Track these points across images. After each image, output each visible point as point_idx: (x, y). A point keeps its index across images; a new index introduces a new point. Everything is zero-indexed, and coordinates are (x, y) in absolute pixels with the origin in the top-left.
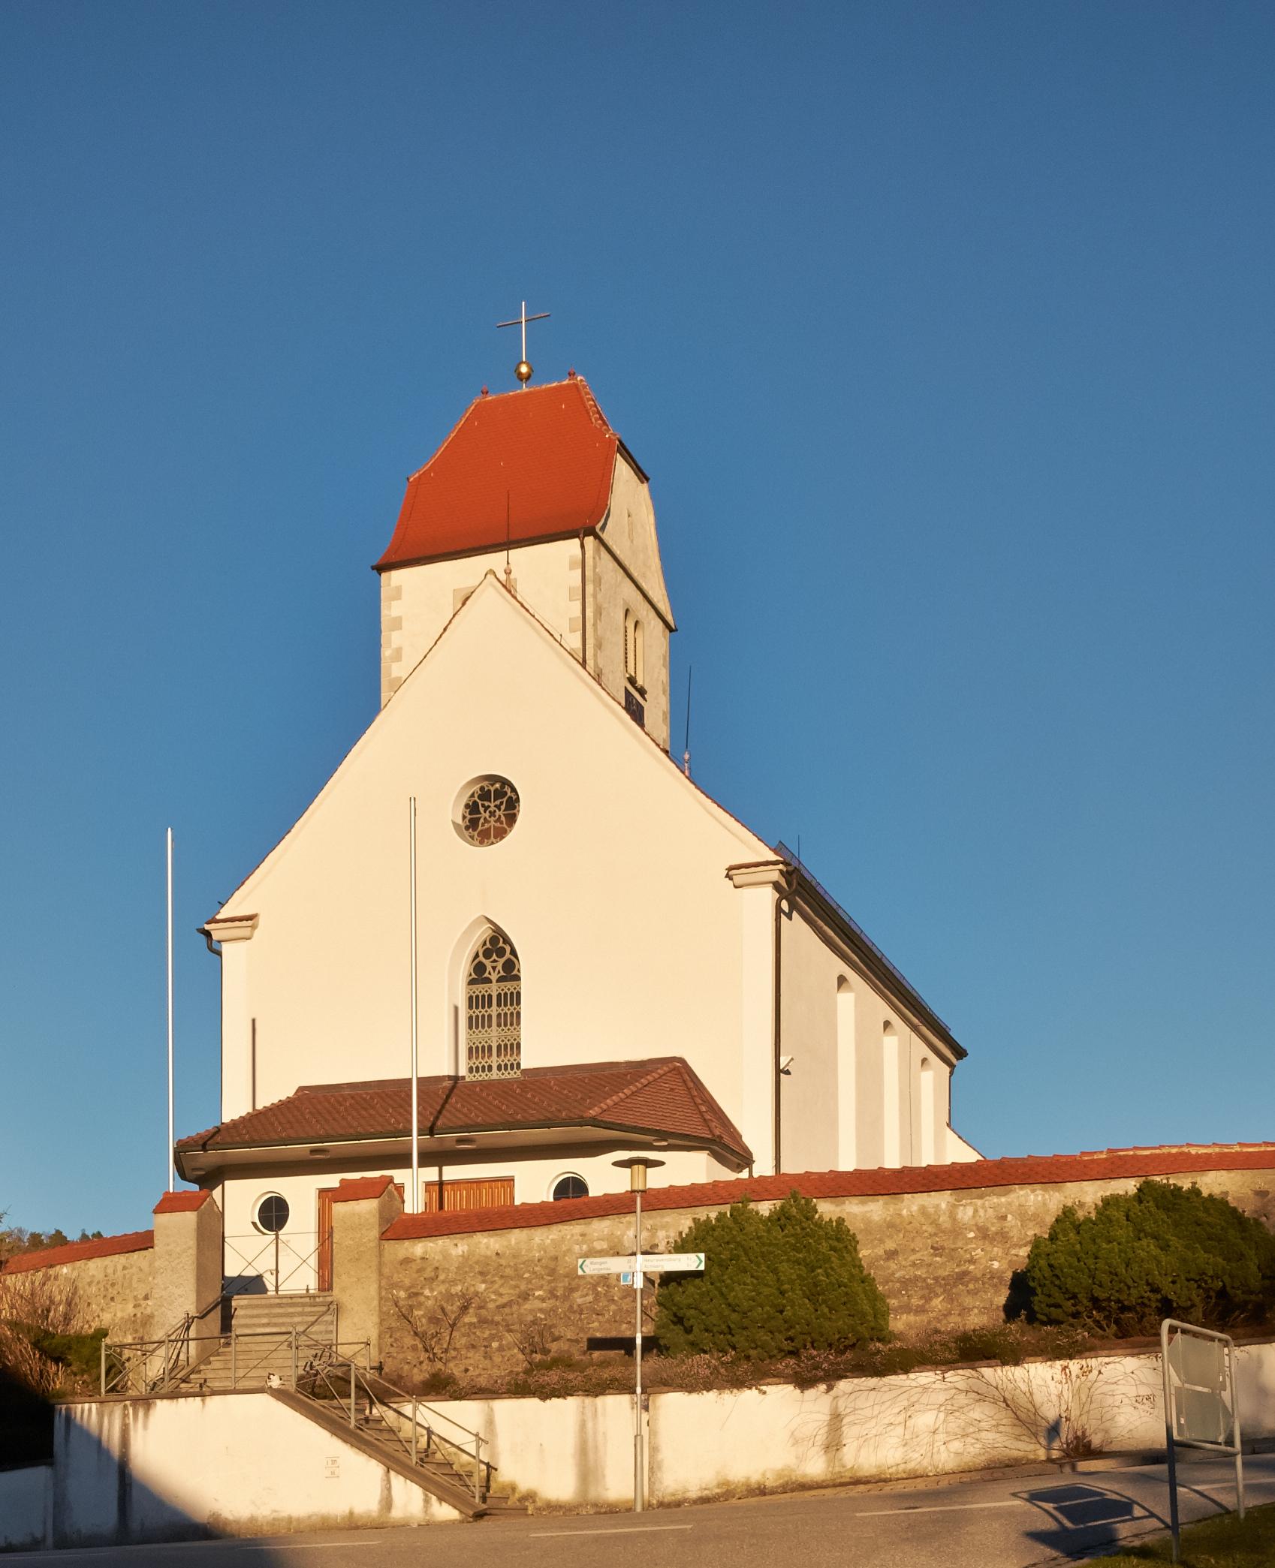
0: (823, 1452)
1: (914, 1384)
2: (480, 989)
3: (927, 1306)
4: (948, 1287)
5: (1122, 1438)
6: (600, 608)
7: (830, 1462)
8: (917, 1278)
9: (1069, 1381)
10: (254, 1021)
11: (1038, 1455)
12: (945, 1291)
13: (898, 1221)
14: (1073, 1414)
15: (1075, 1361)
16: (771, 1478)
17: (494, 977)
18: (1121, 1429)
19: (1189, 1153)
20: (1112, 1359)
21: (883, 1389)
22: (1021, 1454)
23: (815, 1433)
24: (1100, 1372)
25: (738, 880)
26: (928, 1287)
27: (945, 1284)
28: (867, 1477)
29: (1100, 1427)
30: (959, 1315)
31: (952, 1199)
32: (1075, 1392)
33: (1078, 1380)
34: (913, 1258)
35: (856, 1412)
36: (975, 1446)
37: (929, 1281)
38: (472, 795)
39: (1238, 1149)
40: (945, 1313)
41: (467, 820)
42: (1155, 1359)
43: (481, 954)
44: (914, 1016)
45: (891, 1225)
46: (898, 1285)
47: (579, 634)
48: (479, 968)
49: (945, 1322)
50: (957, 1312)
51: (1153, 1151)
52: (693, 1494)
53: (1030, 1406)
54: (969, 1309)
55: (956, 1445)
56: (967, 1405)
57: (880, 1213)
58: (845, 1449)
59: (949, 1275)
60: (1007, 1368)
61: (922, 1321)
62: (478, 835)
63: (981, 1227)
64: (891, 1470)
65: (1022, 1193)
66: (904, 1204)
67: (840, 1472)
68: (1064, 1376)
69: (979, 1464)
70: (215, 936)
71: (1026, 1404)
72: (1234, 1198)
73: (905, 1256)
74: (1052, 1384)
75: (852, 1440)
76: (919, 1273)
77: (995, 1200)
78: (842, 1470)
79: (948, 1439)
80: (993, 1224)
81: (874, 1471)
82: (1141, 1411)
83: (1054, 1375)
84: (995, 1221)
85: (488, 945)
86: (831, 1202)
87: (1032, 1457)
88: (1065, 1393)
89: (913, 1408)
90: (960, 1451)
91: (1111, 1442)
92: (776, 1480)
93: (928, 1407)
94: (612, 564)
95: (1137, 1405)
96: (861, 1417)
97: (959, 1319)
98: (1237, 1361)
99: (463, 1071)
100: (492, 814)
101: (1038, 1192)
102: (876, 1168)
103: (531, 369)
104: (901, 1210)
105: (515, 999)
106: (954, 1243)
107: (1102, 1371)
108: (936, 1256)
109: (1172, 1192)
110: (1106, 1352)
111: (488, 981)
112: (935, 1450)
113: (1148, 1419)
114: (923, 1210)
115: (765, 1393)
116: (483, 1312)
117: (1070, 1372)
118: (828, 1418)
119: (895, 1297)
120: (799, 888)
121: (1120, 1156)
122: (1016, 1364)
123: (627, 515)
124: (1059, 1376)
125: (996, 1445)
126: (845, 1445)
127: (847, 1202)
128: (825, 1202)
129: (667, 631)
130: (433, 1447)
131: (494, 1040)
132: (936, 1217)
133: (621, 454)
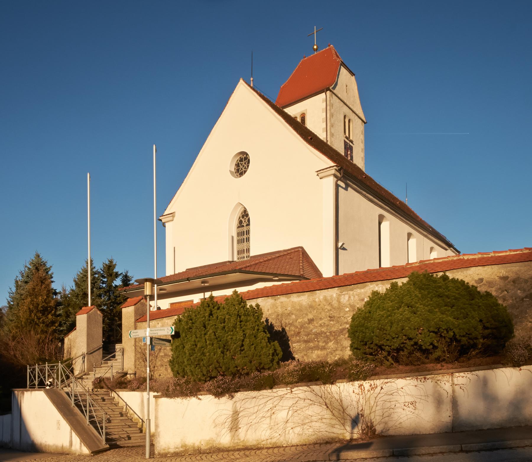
0: (229, 431)
1: (275, 395)
2: (241, 229)
3: (326, 346)
4: (336, 337)
5: (395, 427)
6: (333, 114)
7: (233, 436)
8: (322, 332)
9: (363, 393)
10: (174, 248)
11: (345, 437)
12: (334, 338)
13: (314, 304)
14: (365, 413)
15: (367, 381)
16: (203, 445)
17: (245, 225)
18: (394, 422)
19: (464, 259)
20: (389, 380)
21: (259, 398)
22: (335, 435)
23: (225, 421)
24: (382, 388)
25: (321, 175)
26: (327, 337)
27: (335, 335)
28: (251, 446)
29: (382, 421)
30: (341, 350)
31: (338, 292)
32: (367, 400)
33: (369, 392)
34: (320, 322)
35: (246, 410)
36: (309, 430)
37: (328, 334)
38: (237, 161)
39: (493, 255)
40: (335, 349)
41: (236, 170)
42: (416, 380)
43: (241, 217)
44: (424, 231)
45: (311, 307)
46: (313, 336)
47: (325, 123)
48: (241, 222)
49: (334, 354)
50: (340, 349)
51: (444, 260)
52: (172, 450)
53: (340, 408)
54: (345, 347)
55: (298, 430)
56: (305, 407)
57: (306, 301)
58: (240, 430)
59: (337, 330)
60: (327, 385)
61: (324, 354)
62: (239, 174)
63: (352, 305)
64: (263, 443)
65: (371, 286)
66: (317, 296)
67: (237, 443)
68: (360, 391)
69: (311, 441)
70: (163, 221)
71: (338, 406)
72: (486, 282)
73: (317, 322)
74: (353, 395)
75: (244, 425)
76: (323, 330)
77: (359, 291)
78: (239, 442)
79: (294, 426)
80: (358, 303)
81: (254, 443)
82: (407, 411)
83: (354, 390)
84: (359, 302)
85: (243, 214)
86: (285, 297)
87: (341, 437)
88: (361, 400)
89: (275, 408)
90: (300, 433)
91: (389, 430)
92: (206, 446)
93: (284, 408)
94: (338, 100)
95: (405, 407)
96: (248, 413)
97: (341, 353)
98: (470, 381)
99: (236, 259)
100: (243, 166)
101: (380, 285)
102: (184, 270)
103: (318, 47)
104: (315, 299)
105: (248, 232)
106: (339, 314)
107: (383, 388)
108: (331, 321)
109: (460, 282)
110: (385, 376)
111: (243, 226)
112: (287, 432)
113: (412, 416)
114: (325, 299)
115: (201, 399)
116: (165, 351)
117: (364, 388)
118: (231, 413)
119: (312, 342)
120: (345, 175)
121: (426, 264)
122: (332, 383)
123: (345, 86)
124: (357, 390)
125: (321, 430)
126: (240, 428)
127: (292, 296)
128: (283, 297)
129: (363, 123)
130: (127, 411)
131: (245, 247)
132: (331, 301)
133: (343, 66)
